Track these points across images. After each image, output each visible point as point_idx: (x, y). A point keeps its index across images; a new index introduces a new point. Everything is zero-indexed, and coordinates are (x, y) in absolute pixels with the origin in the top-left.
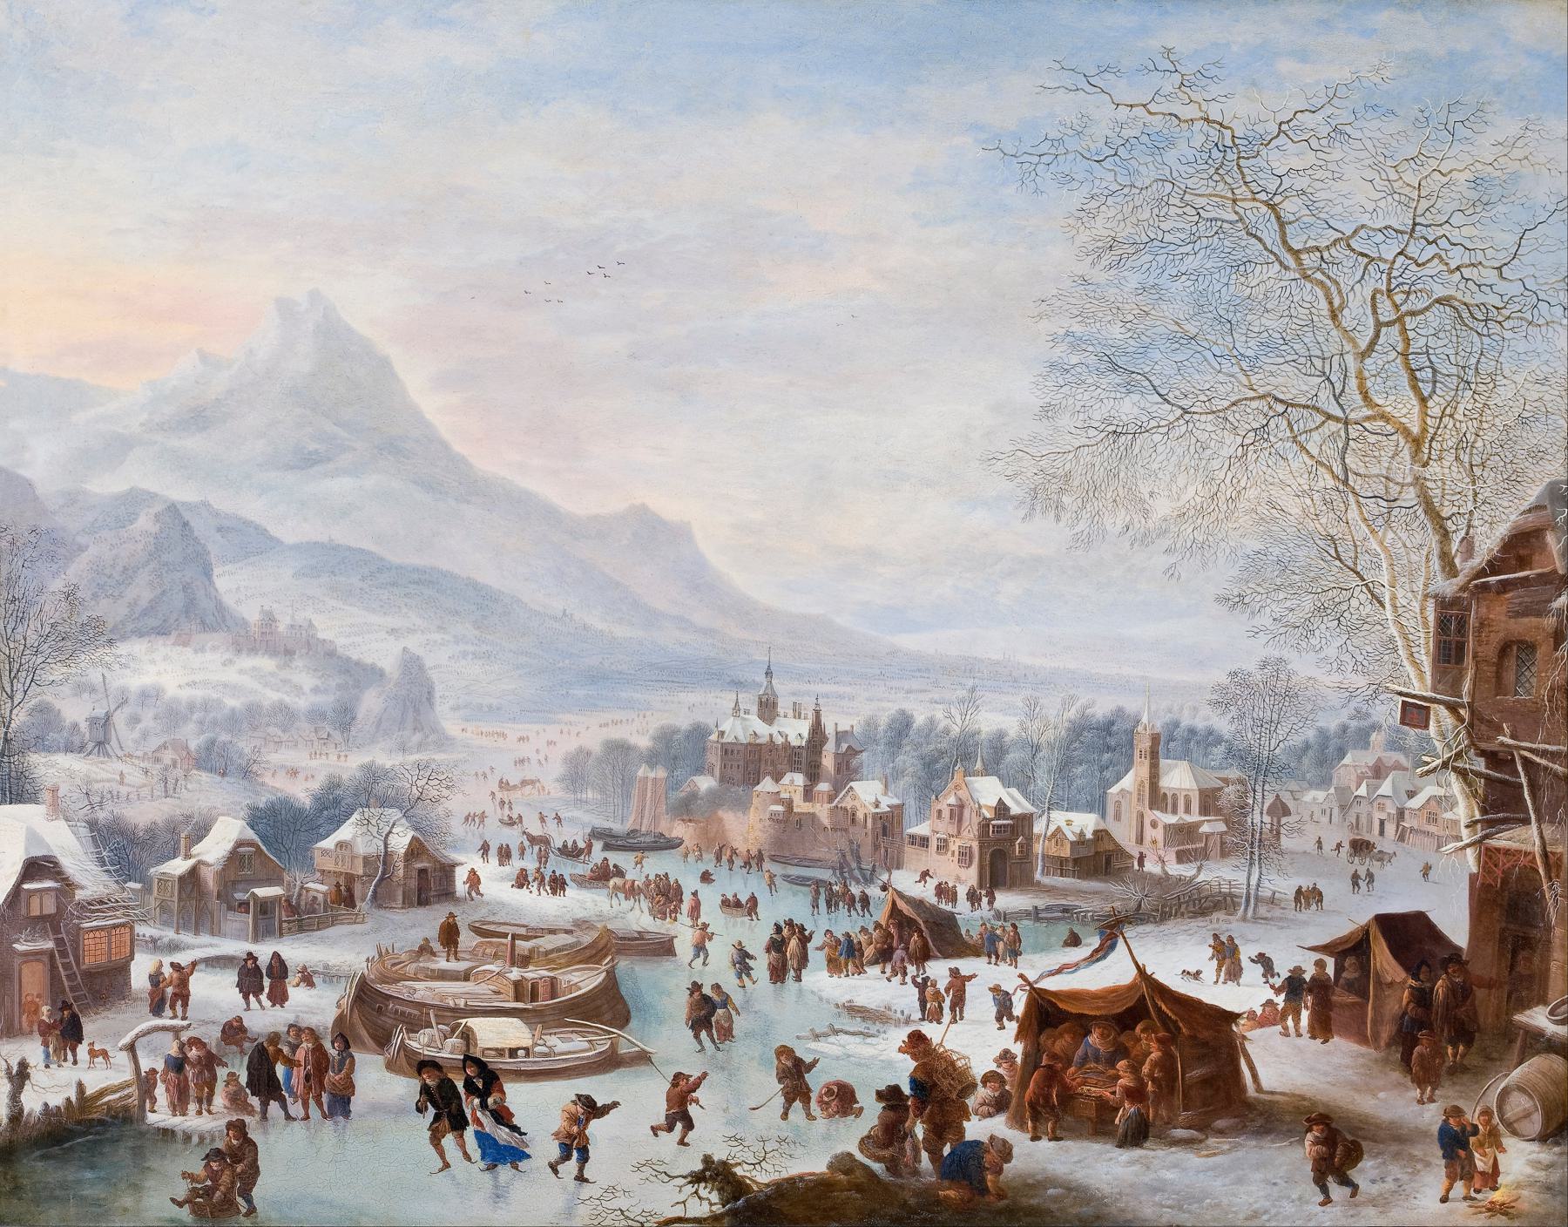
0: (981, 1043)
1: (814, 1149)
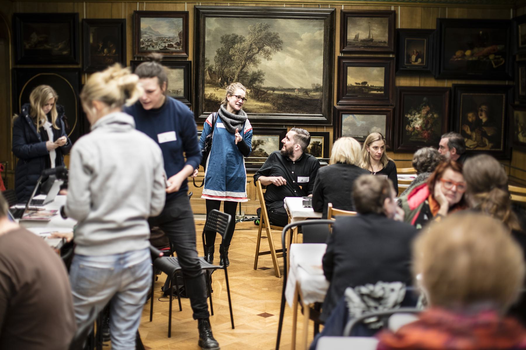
0: (167, 45)
1: (162, 48)
